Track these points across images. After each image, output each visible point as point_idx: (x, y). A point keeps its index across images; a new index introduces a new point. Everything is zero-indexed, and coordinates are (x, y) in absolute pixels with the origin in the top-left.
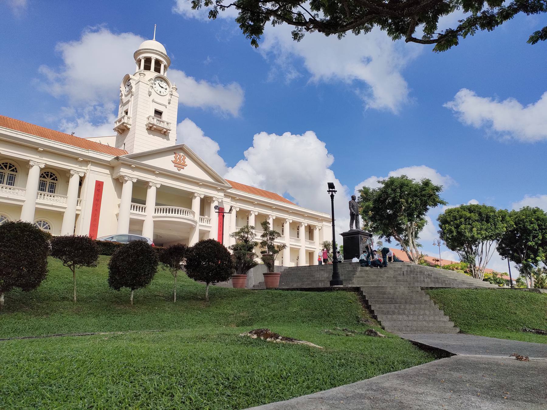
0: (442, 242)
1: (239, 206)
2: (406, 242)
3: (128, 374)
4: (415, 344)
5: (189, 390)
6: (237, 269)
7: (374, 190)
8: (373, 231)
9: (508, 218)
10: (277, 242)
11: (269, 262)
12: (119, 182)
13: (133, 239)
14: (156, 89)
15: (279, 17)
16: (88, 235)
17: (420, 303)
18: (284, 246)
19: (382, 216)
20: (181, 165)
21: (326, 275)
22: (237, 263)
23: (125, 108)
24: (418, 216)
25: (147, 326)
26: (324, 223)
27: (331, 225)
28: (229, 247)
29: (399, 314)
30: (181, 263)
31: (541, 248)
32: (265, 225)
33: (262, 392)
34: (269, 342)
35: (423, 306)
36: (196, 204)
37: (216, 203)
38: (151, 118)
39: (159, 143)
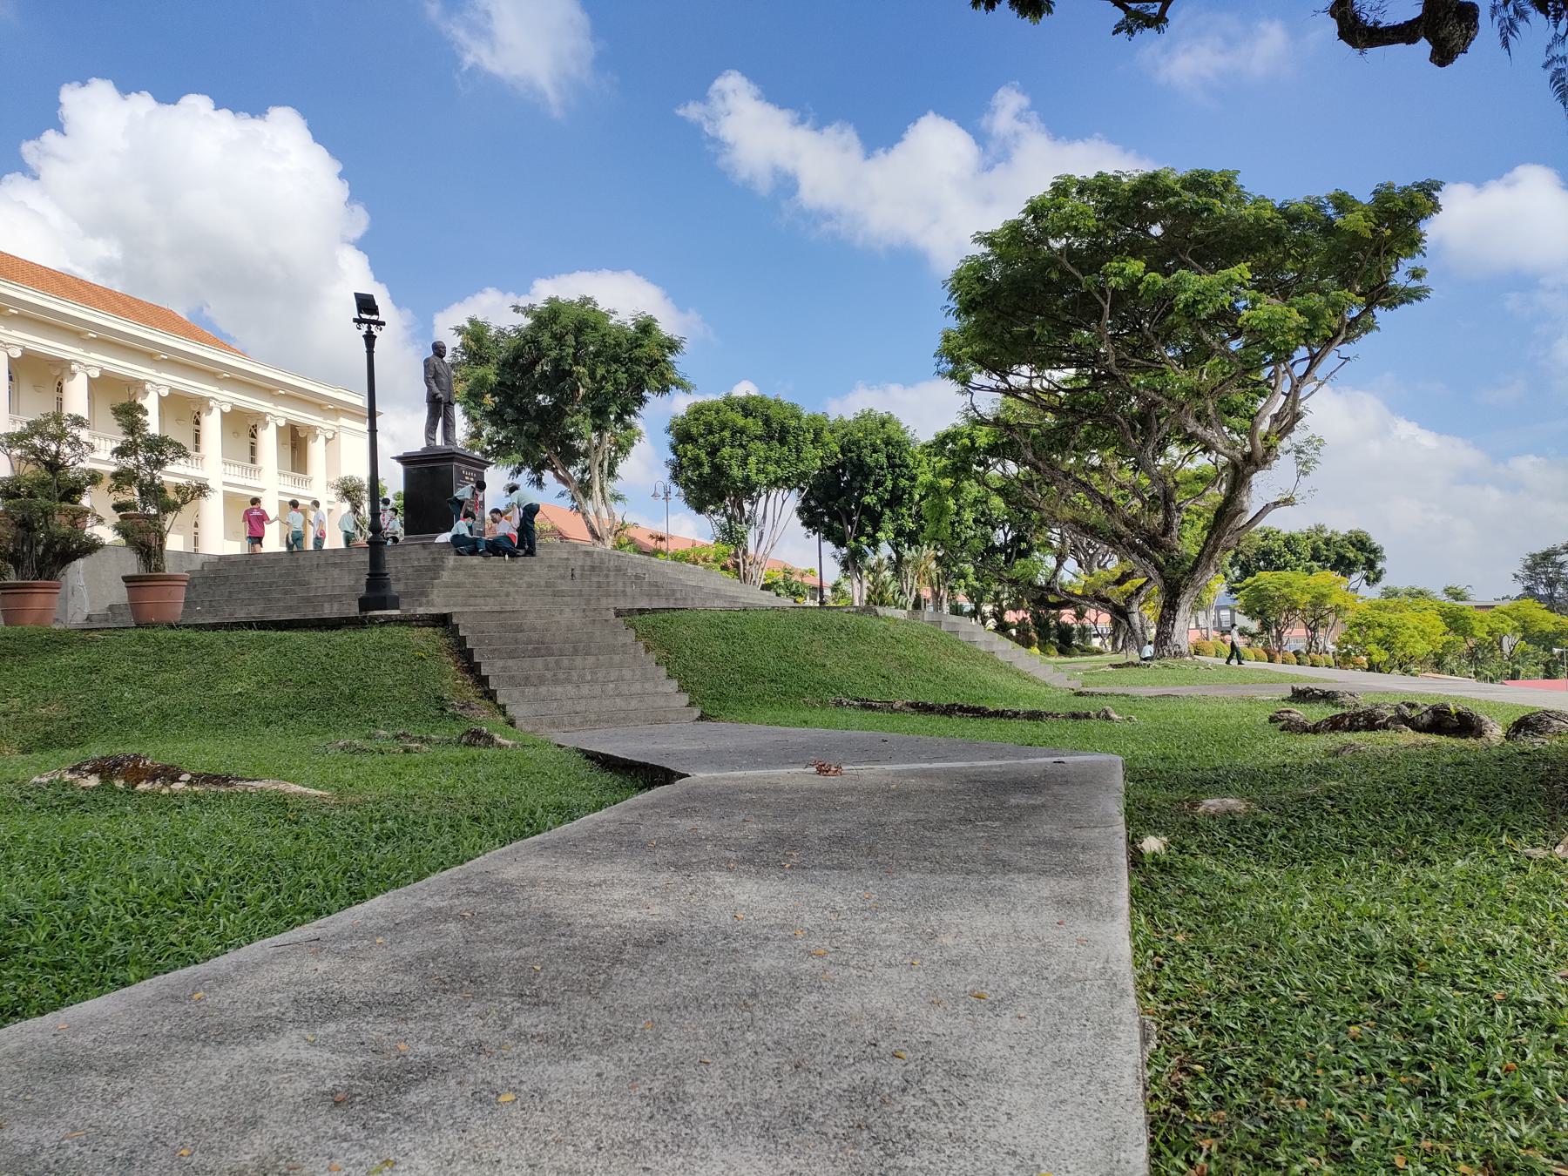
0: (675, 489)
2: (585, 489)
4: (591, 756)
7: (501, 332)
8: (495, 453)
9: (827, 437)
10: (174, 473)
17: (612, 650)
18: (201, 490)
19: (522, 410)
24: (619, 418)
26: (343, 421)
27: (365, 427)
29: (556, 681)
31: (887, 511)
32: (129, 414)
33: (117, 948)
34: (145, 793)
35: (617, 658)
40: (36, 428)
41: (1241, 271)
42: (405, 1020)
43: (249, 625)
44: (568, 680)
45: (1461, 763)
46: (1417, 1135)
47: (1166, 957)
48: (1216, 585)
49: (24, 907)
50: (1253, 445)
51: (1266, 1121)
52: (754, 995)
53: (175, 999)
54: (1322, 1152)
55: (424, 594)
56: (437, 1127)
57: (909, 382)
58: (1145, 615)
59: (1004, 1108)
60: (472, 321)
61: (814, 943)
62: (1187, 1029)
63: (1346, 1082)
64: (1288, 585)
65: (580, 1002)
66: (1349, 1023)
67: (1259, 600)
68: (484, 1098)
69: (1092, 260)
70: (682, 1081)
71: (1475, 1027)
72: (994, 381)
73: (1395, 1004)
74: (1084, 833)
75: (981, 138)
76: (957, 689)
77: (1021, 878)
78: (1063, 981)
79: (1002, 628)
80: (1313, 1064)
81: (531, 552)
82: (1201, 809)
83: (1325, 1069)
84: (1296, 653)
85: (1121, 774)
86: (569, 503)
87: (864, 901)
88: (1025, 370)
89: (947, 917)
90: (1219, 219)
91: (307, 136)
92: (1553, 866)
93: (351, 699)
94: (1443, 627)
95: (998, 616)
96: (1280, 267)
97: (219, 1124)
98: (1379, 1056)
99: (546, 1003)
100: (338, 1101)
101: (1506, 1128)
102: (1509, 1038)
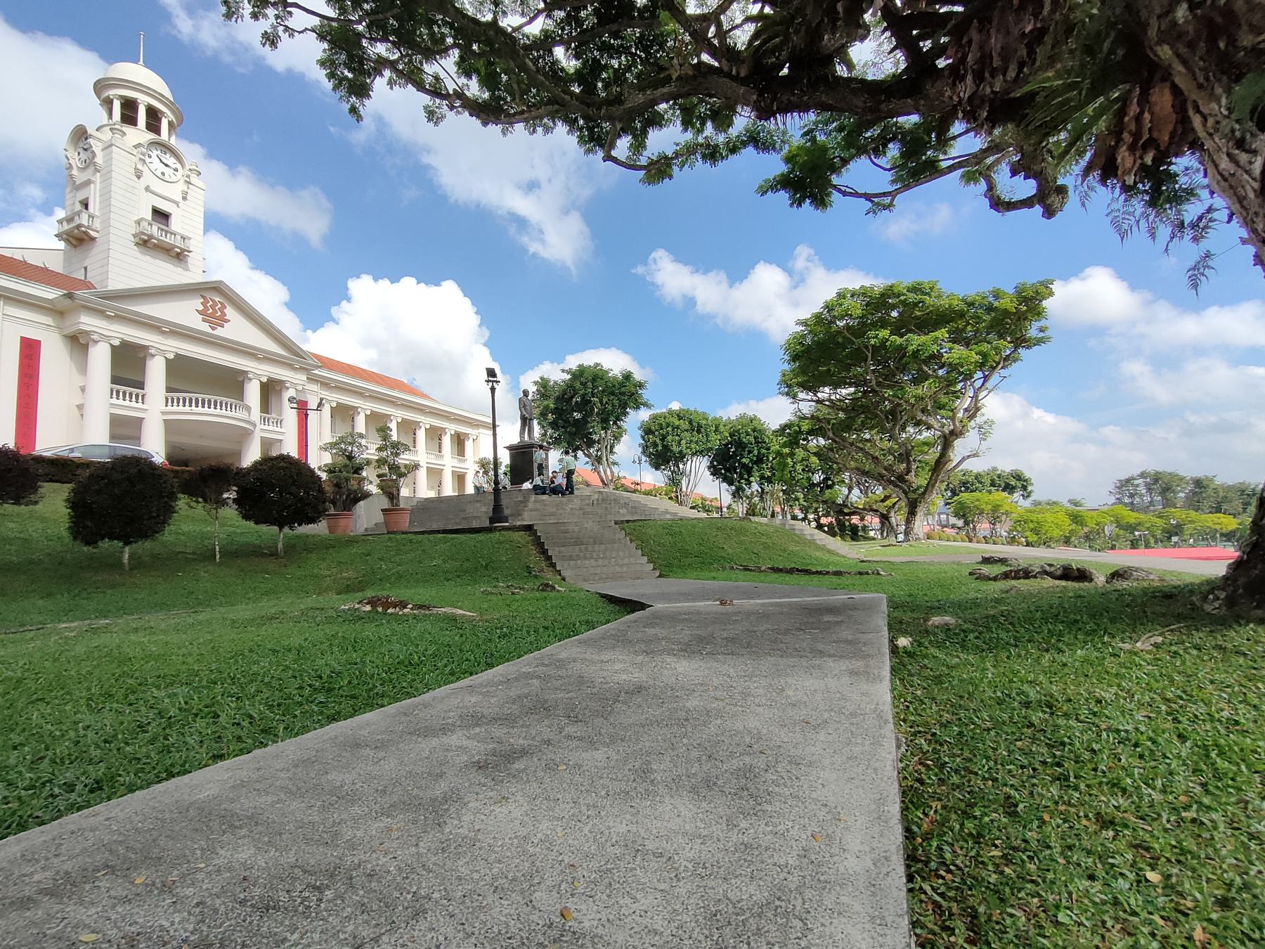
0: (644, 458)
1: (336, 398)
2: (599, 460)
3: (123, 691)
4: (604, 596)
5: (247, 703)
6: (334, 503)
7: (555, 382)
8: (554, 443)
9: (722, 428)
10: (404, 459)
11: (391, 492)
12: (79, 343)
13: (120, 453)
14: (153, 167)
15: (400, 73)
16: (12, 445)
17: (614, 542)
18: (416, 466)
19: (566, 421)
20: (222, 321)
21: (484, 509)
22: (335, 493)
23: (81, 195)
24: (615, 423)
25: (162, 606)
26: (481, 430)
27: (491, 433)
28: (320, 468)
29: (585, 558)
30: (225, 496)
31: (755, 466)
32: (384, 431)
33: (379, 689)
34: (392, 614)
35: (616, 546)
36: (253, 393)
37: (291, 393)
38: (144, 224)
39: (162, 273)
40: (342, 440)
41: (942, 333)
42: (513, 727)
43: (439, 532)
44: (592, 558)
45: (1080, 597)
46: (1056, 803)
47: (911, 702)
48: (937, 500)
49: (338, 668)
50: (954, 425)
51: (969, 793)
52: (687, 720)
53: (405, 714)
54: (1001, 811)
55: (520, 515)
56: (528, 781)
57: (760, 399)
58: (898, 519)
59: (820, 781)
60: (542, 378)
61: (719, 694)
62: (923, 741)
63: (1015, 773)
64: (978, 500)
65: (598, 721)
66: (1016, 740)
67: (962, 508)
68: (551, 767)
69: (861, 329)
70: (650, 763)
71: (1090, 743)
72: (810, 396)
73: (1042, 730)
74: (865, 636)
75: (789, 272)
76: (796, 559)
77: (830, 660)
78: (854, 715)
79: (820, 527)
80: (996, 763)
81: (572, 493)
82: (930, 623)
83: (1003, 765)
84: (984, 537)
85: (886, 604)
86: (591, 467)
87: (745, 671)
88: (827, 389)
89: (789, 680)
90: (928, 307)
91: (460, 294)
92: (1135, 654)
93: (486, 567)
94: (1069, 522)
95: (817, 520)
96: (964, 330)
97: (425, 776)
98: (1034, 758)
99: (581, 721)
100: (481, 766)
101: (1109, 801)
102: (1111, 750)
